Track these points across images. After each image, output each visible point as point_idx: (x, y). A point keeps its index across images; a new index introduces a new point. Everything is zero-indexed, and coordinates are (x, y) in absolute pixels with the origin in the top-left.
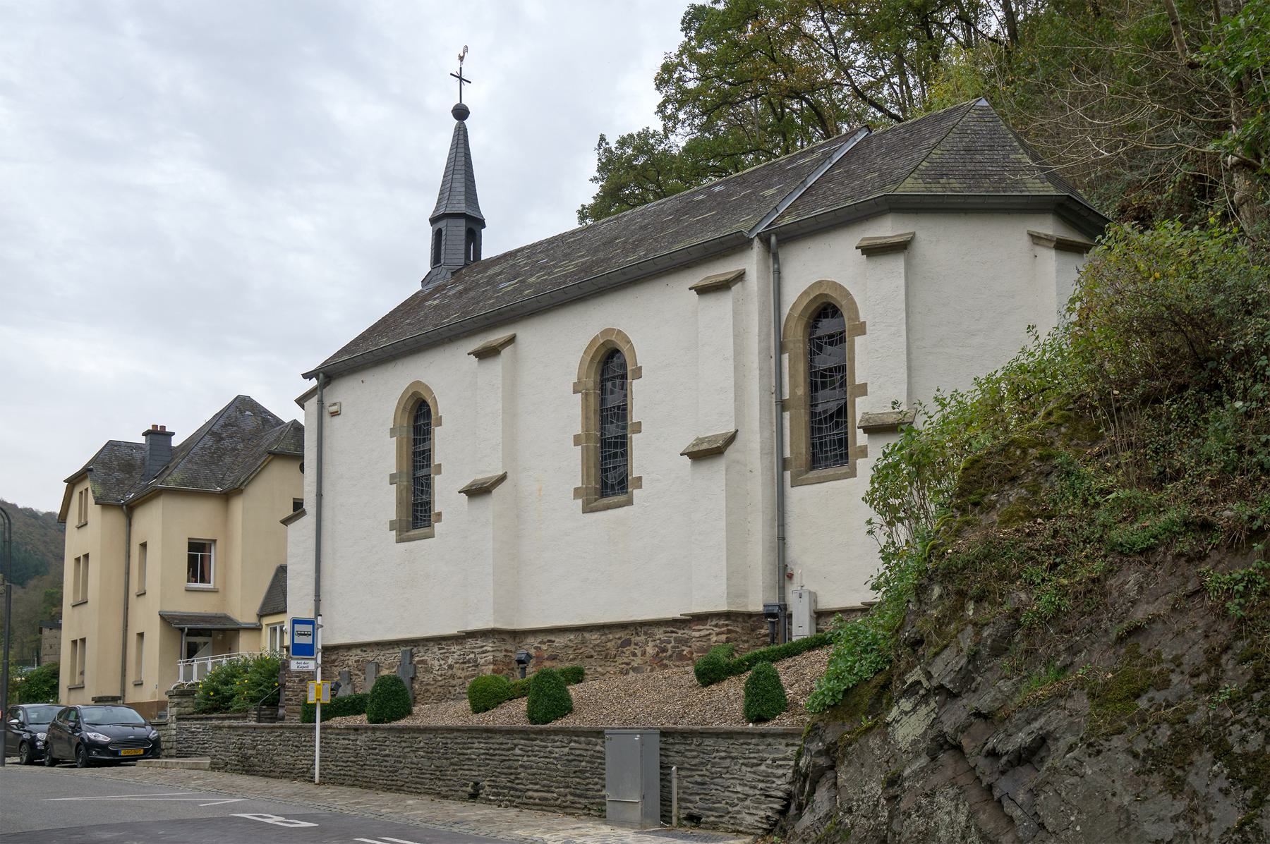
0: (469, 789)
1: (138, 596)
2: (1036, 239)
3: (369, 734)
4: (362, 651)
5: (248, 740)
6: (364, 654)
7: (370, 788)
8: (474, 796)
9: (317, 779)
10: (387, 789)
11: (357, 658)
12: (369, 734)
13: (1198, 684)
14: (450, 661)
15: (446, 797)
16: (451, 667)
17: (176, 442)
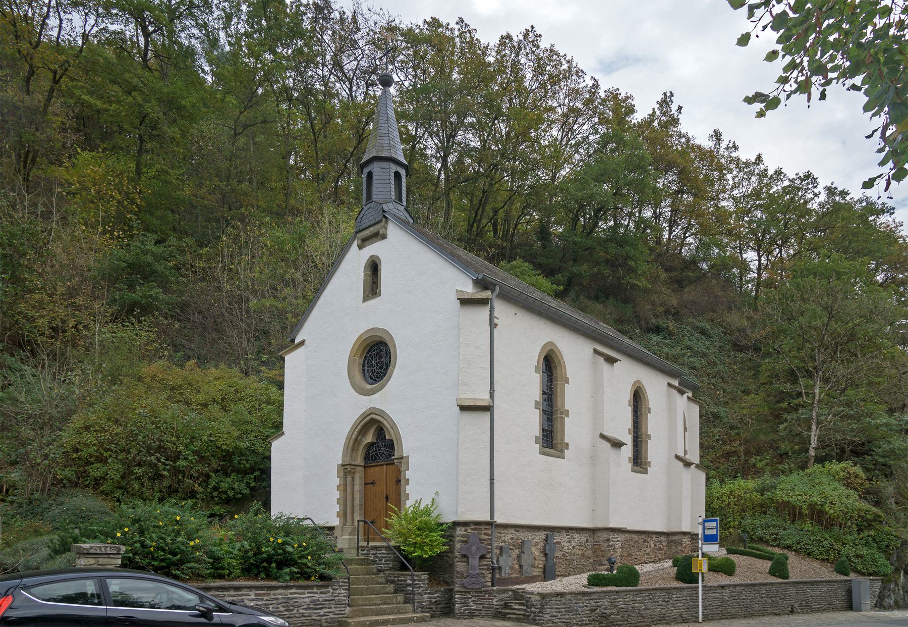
0: (790, 609)
1: (463, 408)
2: (670, 385)
3: (731, 588)
4: (515, 530)
5: (606, 602)
6: (517, 534)
7: (733, 618)
8: (792, 612)
9: (700, 621)
10: (745, 617)
11: (511, 536)
12: (731, 588)
13: (64, 553)
14: (573, 544)
15: (779, 615)
16: (574, 547)
17: (638, 117)
